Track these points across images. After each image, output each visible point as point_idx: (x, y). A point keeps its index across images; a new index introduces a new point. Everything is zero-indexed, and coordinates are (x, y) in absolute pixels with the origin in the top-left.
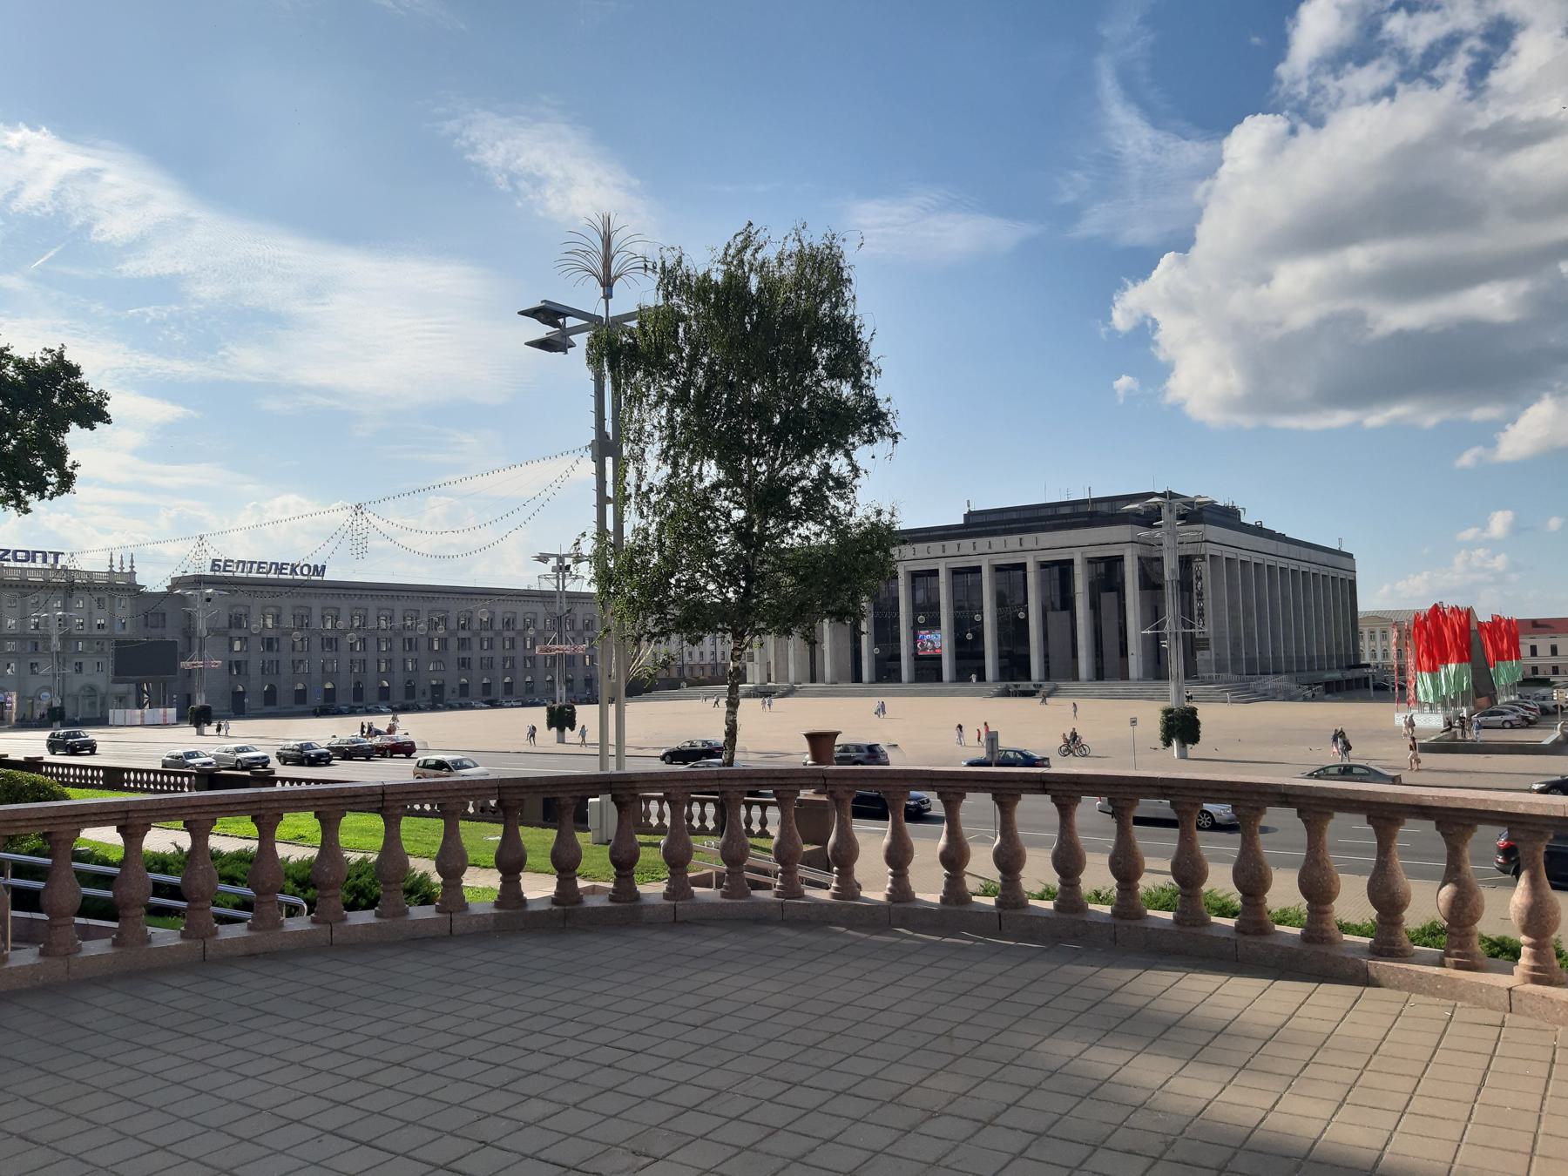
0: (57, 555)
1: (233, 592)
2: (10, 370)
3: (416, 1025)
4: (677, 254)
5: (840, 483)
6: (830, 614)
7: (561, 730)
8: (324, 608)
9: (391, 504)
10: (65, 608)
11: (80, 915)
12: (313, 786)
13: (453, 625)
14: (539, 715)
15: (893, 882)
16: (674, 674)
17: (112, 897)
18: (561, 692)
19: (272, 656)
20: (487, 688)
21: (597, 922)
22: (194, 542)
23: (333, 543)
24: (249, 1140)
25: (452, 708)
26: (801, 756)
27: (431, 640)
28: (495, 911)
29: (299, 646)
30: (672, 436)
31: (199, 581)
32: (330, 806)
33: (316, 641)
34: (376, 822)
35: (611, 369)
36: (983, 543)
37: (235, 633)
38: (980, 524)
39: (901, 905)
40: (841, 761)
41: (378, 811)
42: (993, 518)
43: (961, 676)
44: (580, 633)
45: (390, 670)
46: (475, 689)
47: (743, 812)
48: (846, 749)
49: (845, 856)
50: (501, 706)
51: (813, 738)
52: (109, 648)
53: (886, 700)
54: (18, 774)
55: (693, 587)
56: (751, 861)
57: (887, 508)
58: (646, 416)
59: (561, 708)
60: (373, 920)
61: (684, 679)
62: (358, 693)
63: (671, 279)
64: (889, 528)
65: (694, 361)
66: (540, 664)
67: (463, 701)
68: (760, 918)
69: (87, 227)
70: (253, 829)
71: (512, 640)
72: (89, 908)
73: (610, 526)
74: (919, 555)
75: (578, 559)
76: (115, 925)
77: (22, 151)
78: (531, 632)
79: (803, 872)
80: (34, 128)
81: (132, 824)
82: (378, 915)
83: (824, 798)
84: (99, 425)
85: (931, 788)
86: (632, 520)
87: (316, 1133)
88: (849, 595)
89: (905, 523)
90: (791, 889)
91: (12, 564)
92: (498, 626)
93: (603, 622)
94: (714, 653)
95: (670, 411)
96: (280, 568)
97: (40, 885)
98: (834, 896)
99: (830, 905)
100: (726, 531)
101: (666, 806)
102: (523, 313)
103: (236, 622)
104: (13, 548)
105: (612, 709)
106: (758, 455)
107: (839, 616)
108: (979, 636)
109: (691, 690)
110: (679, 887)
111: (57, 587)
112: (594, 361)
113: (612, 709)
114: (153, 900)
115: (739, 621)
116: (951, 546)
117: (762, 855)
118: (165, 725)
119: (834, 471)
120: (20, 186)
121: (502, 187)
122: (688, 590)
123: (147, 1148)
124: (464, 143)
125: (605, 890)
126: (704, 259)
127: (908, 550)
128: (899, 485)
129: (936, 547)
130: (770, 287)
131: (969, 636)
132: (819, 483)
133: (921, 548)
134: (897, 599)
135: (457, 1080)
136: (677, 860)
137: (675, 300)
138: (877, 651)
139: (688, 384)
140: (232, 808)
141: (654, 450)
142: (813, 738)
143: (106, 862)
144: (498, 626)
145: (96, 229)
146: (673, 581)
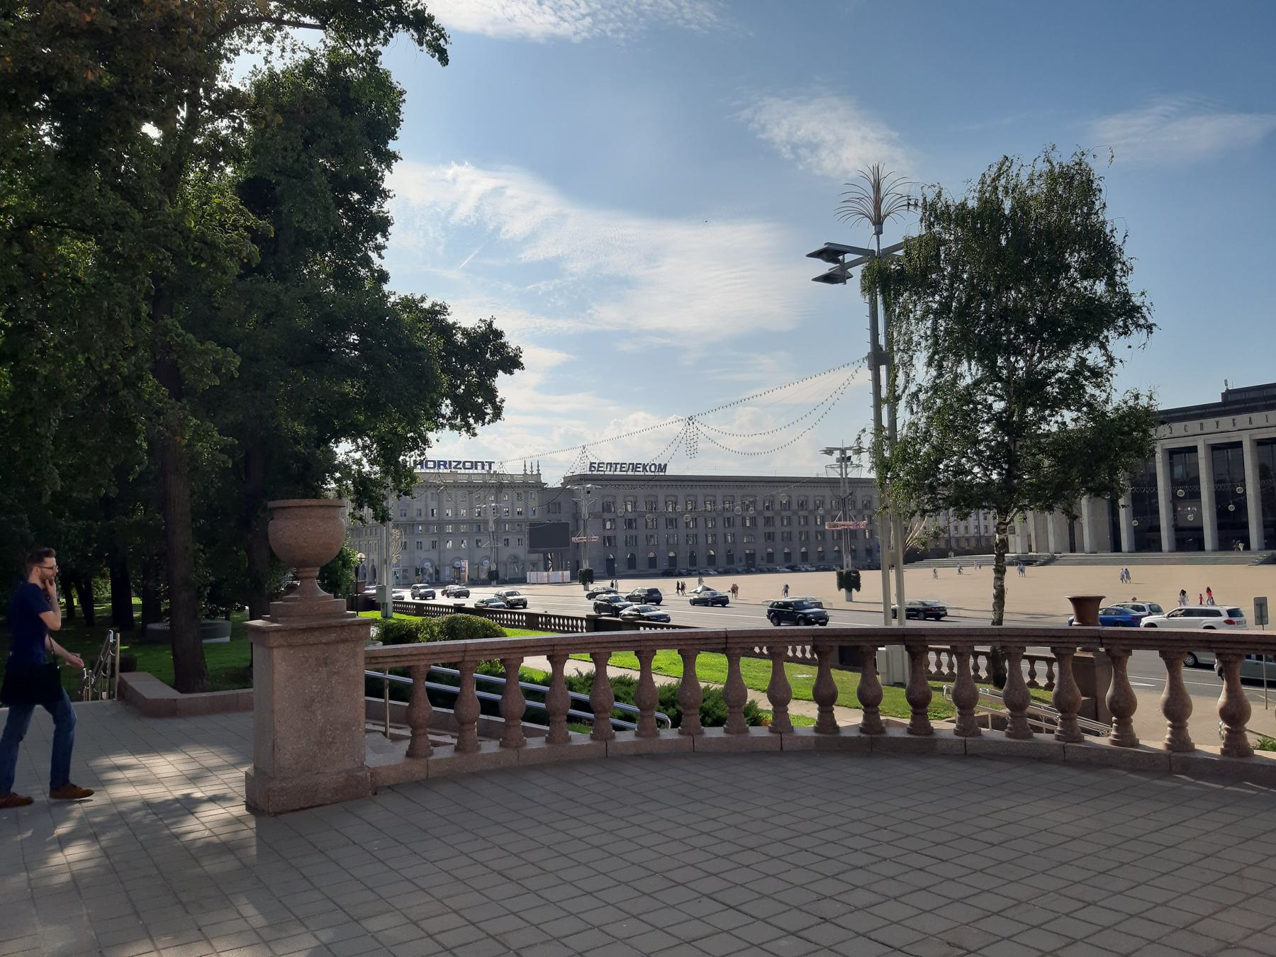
0: (490, 463)
1: (603, 483)
2: (459, 337)
3: (763, 820)
4: (937, 190)
5: (1096, 373)
6: (1089, 490)
7: (849, 590)
8: (706, 496)
9: (710, 415)
10: (496, 501)
11: (524, 720)
12: (677, 630)
13: (760, 507)
14: (831, 578)
15: (1172, 733)
16: (942, 545)
17: (545, 707)
18: (847, 559)
19: (632, 532)
20: (788, 557)
21: (897, 749)
22: (579, 451)
23: (672, 449)
24: (649, 895)
25: (762, 572)
26: (1065, 616)
27: (744, 519)
28: (814, 734)
29: (650, 524)
30: (936, 343)
31: (583, 479)
32: (691, 644)
33: (662, 521)
34: (722, 660)
35: (882, 292)
36: (1242, 420)
37: (606, 516)
38: (1238, 402)
39: (1182, 755)
40: (1105, 622)
41: (723, 651)
42: (1253, 395)
43: (1225, 544)
44: (860, 512)
45: (714, 542)
46: (779, 557)
47: (972, 660)
48: (1107, 611)
49: (1123, 708)
50: (800, 571)
51: (1078, 602)
52: (526, 528)
53: (1131, 568)
54: (473, 617)
55: (960, 471)
56: (1030, 709)
57: (1144, 392)
58: (913, 328)
59: (848, 573)
60: (723, 735)
61: (951, 549)
62: (693, 559)
63: (935, 213)
64: (1148, 411)
65: (955, 277)
66: (829, 537)
67: (770, 566)
68: (1040, 757)
69: (497, 230)
70: (636, 662)
71: (806, 518)
72: (532, 715)
73: (885, 423)
74: (1175, 434)
75: (859, 451)
76: (547, 728)
77: (454, 180)
78: (821, 511)
79: (1082, 722)
80: (460, 163)
81: (557, 655)
82: (726, 731)
83: (1090, 655)
84: (516, 371)
85: (1210, 649)
86: (903, 416)
87: (697, 895)
88: (1109, 474)
89: (1164, 403)
90: (1070, 734)
91: (463, 471)
92: (794, 506)
93: (882, 501)
94: (978, 527)
95: (935, 322)
96: (635, 467)
97: (499, 697)
98: (1113, 742)
99: (1110, 750)
100: (988, 422)
101: (954, 658)
102: (810, 255)
103: (606, 508)
104: (463, 460)
105: (892, 574)
106: (1016, 354)
107: (1096, 492)
108: (1242, 507)
109: (958, 558)
110: (968, 725)
111: (491, 486)
112: (868, 288)
113: (892, 574)
114: (572, 711)
115: (1003, 499)
116: (1210, 424)
117: (1042, 703)
118: (563, 583)
119: (1090, 362)
120: (455, 205)
121: (787, 156)
122: (956, 474)
123: (579, 892)
124: (756, 126)
125: (902, 725)
126: (961, 191)
127: (1163, 430)
128: (1147, 372)
129: (1193, 426)
130: (1022, 205)
131: (1232, 508)
132: (1074, 374)
133: (1178, 428)
134: (1154, 476)
135: (798, 867)
136: (965, 702)
137: (937, 228)
138: (1135, 523)
139: (951, 297)
140: (622, 645)
141: (921, 358)
142: (1078, 602)
143: (532, 681)
144: (794, 506)
145: (504, 230)
146: (941, 466)
